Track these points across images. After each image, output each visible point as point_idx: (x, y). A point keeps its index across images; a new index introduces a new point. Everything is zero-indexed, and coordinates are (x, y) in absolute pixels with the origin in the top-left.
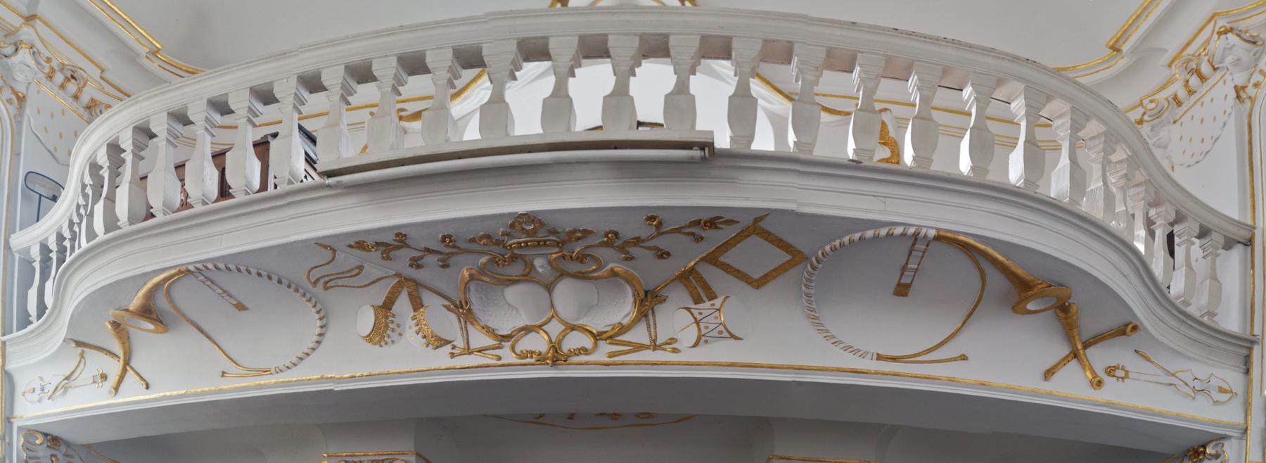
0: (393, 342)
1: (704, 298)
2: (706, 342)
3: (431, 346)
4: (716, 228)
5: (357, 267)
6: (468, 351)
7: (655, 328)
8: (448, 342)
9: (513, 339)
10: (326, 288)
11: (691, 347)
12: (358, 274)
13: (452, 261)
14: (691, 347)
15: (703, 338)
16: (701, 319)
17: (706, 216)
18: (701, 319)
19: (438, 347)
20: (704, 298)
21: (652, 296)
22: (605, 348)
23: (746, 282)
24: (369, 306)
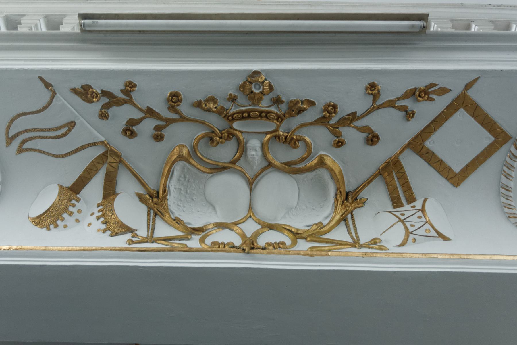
0: (65, 226)
1: (404, 201)
2: (415, 240)
3: (109, 233)
4: (430, 100)
5: (67, 125)
6: (151, 239)
7: (356, 231)
8: (129, 230)
9: (204, 233)
10: (21, 150)
11: (399, 246)
12: (64, 135)
13: (166, 132)
14: (399, 246)
15: (411, 237)
16: (405, 219)
17: (421, 84)
18: (405, 219)
19: (117, 234)
20: (404, 201)
21: (352, 198)
22: (303, 246)
23: (446, 178)
24: (56, 185)
